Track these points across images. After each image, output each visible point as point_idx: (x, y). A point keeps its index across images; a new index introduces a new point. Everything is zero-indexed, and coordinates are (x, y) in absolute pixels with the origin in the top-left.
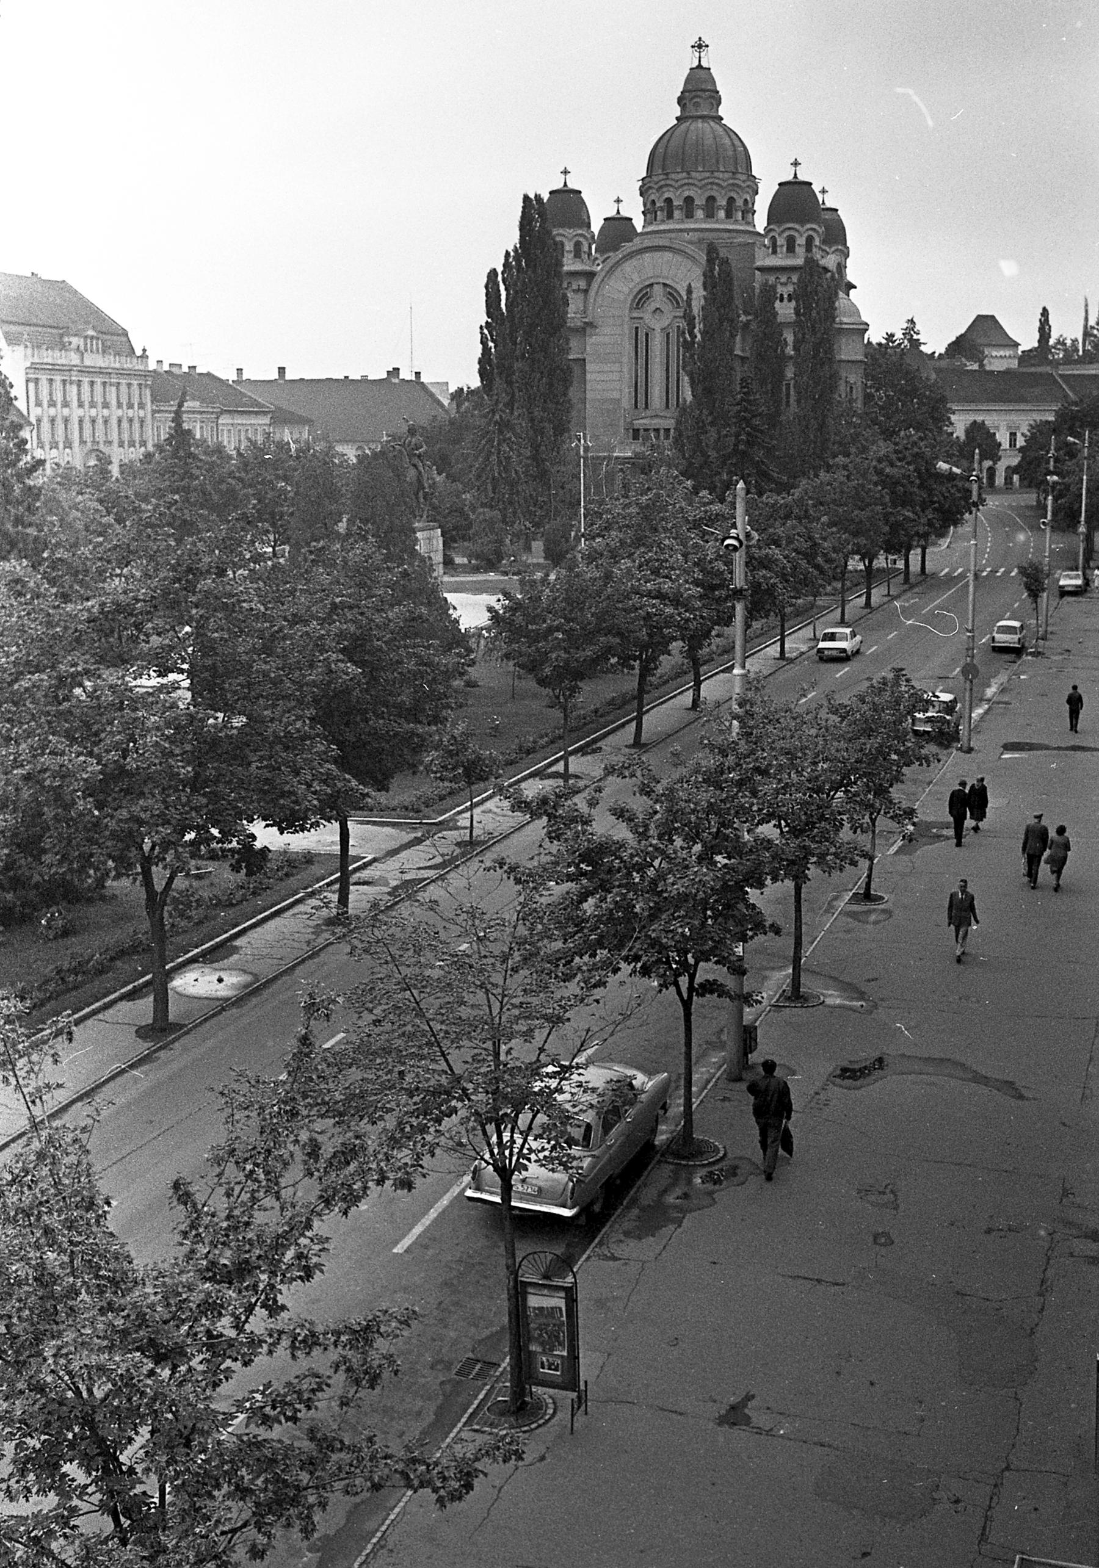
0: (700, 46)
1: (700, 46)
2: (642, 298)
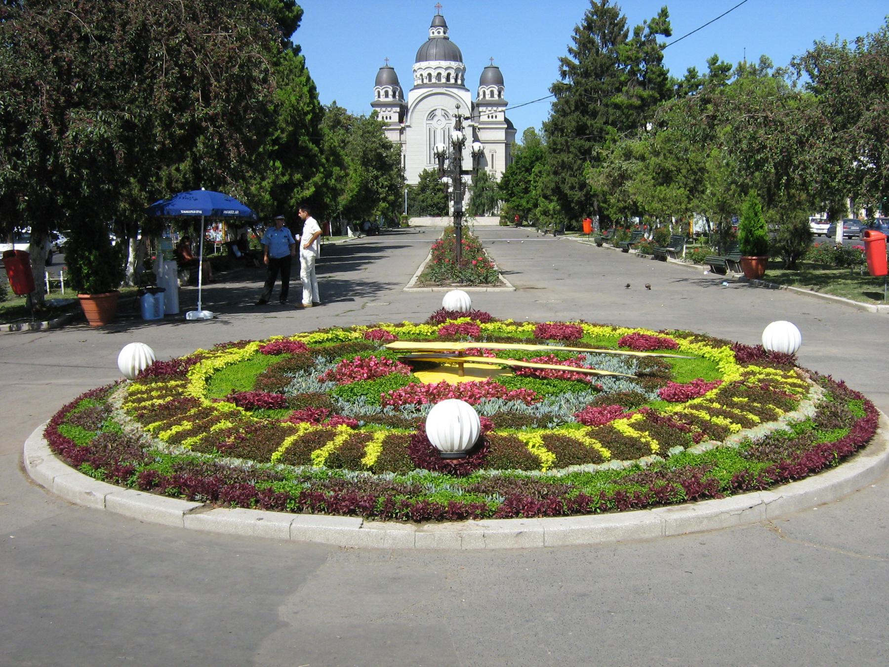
0: (438, 7)
1: (438, 7)
2: (432, 115)
